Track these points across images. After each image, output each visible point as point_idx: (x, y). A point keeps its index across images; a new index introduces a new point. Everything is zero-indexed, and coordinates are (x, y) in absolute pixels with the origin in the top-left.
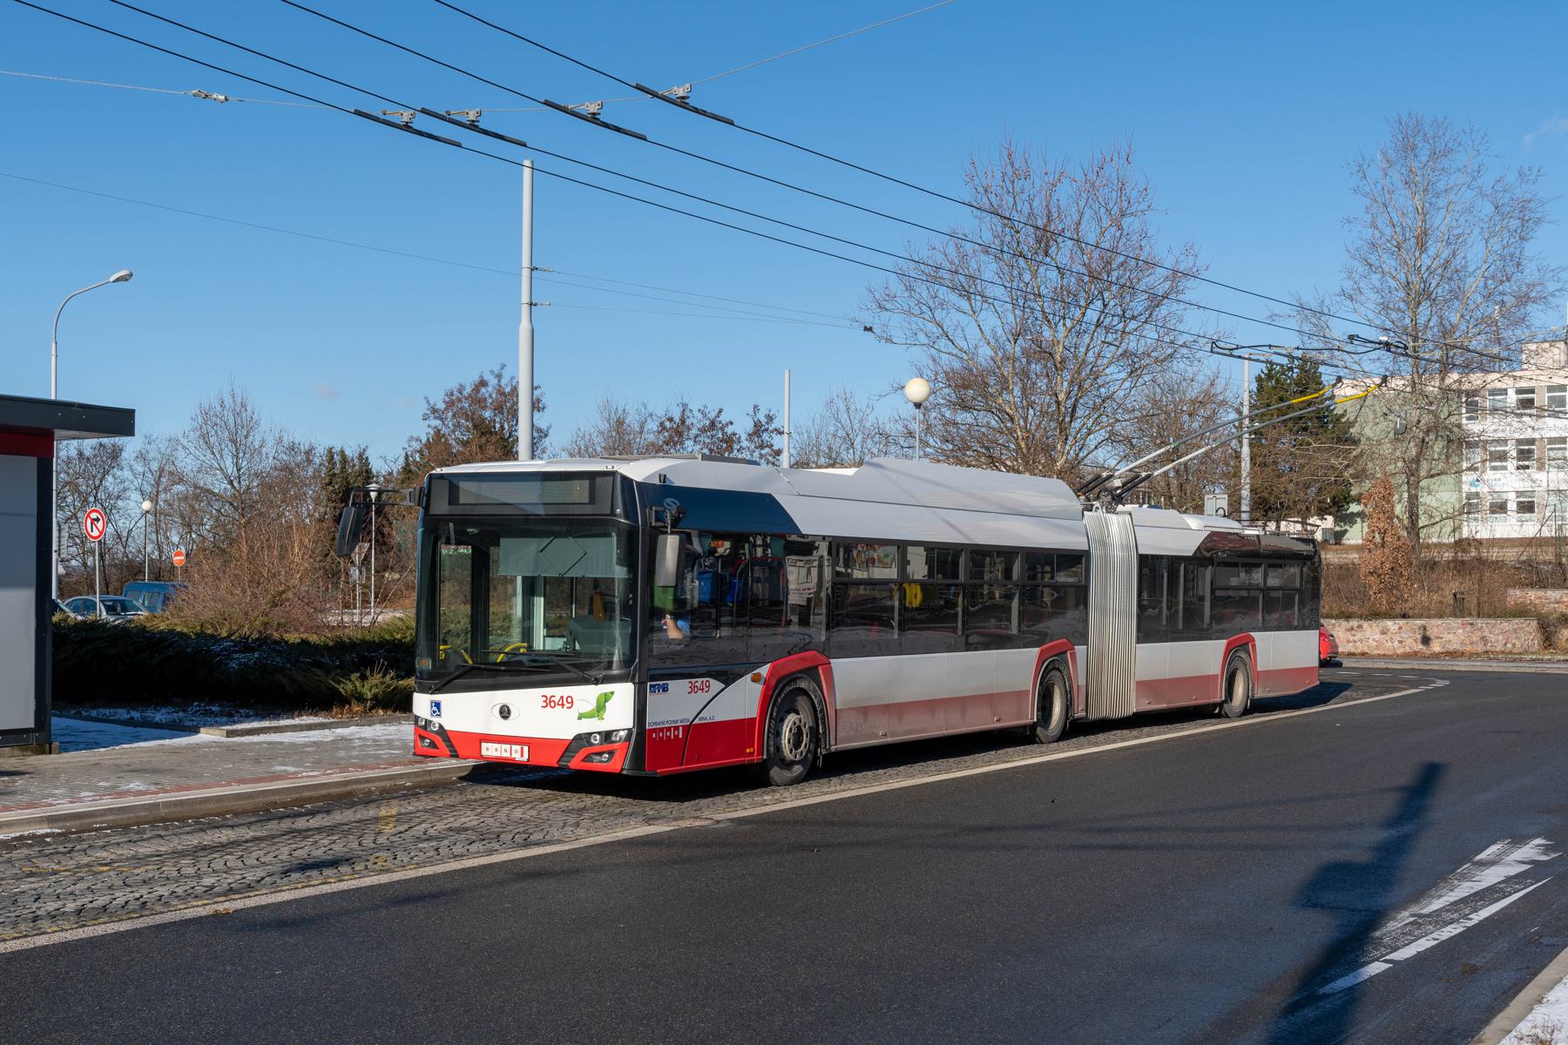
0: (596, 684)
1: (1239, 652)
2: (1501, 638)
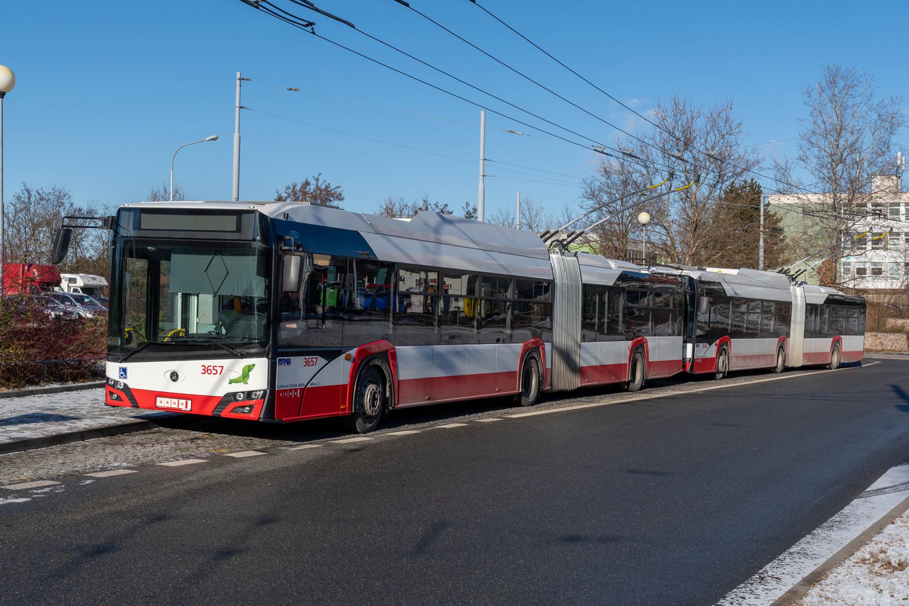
0: (242, 358)
1: (837, 343)
2: (890, 343)
